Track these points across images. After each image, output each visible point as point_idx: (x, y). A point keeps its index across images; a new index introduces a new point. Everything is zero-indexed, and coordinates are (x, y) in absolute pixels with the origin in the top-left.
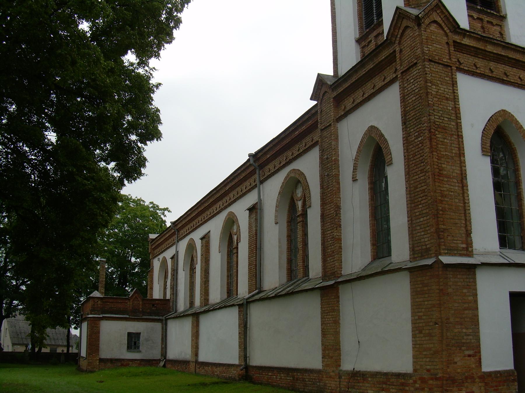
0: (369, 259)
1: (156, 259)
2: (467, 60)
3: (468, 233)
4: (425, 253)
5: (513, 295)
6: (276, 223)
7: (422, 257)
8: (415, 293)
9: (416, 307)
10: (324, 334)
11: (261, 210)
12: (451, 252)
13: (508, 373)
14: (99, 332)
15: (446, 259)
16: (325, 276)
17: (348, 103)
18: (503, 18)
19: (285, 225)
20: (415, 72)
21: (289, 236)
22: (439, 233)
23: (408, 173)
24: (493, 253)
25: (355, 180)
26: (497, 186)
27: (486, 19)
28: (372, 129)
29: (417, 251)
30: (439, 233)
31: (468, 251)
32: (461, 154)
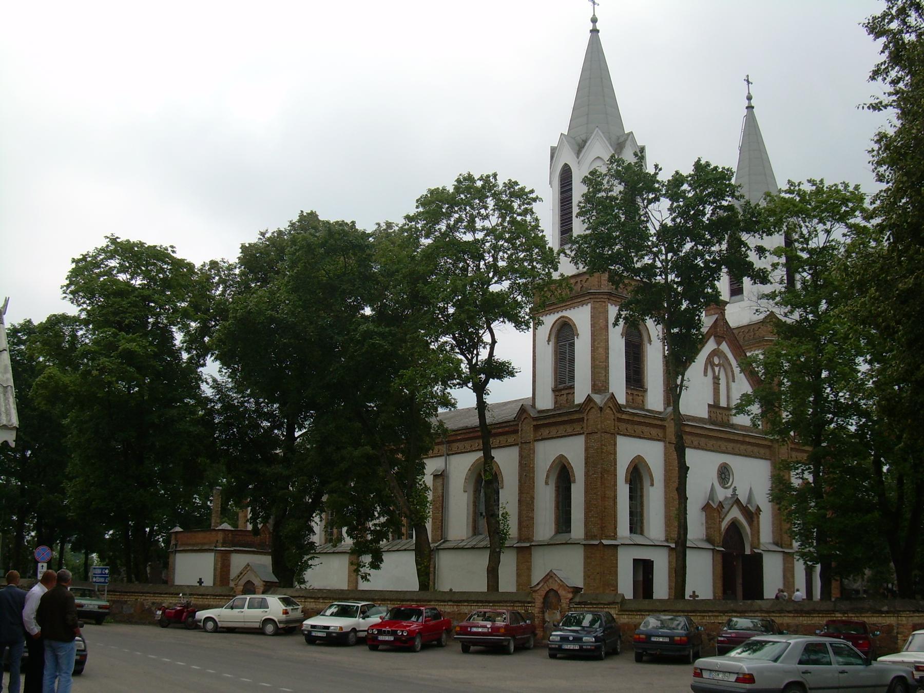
0: (553, 533)
1: (617, 620)
2: (623, 426)
3: (616, 528)
4: (594, 537)
5: (634, 560)
6: (465, 491)
7: (592, 539)
8: (586, 558)
9: (587, 564)
10: (519, 575)
11: (448, 477)
12: (608, 537)
13: (473, 429)
14: (229, 566)
15: (605, 542)
16: (520, 540)
17: (545, 432)
18: (646, 391)
19: (472, 493)
20: (596, 436)
21: (474, 502)
22: (602, 528)
23: (586, 492)
24: (626, 538)
25: (547, 483)
26: (631, 498)
27: (635, 393)
28: (562, 456)
29: (588, 535)
30: (602, 528)
31: (615, 537)
32: (615, 485)
